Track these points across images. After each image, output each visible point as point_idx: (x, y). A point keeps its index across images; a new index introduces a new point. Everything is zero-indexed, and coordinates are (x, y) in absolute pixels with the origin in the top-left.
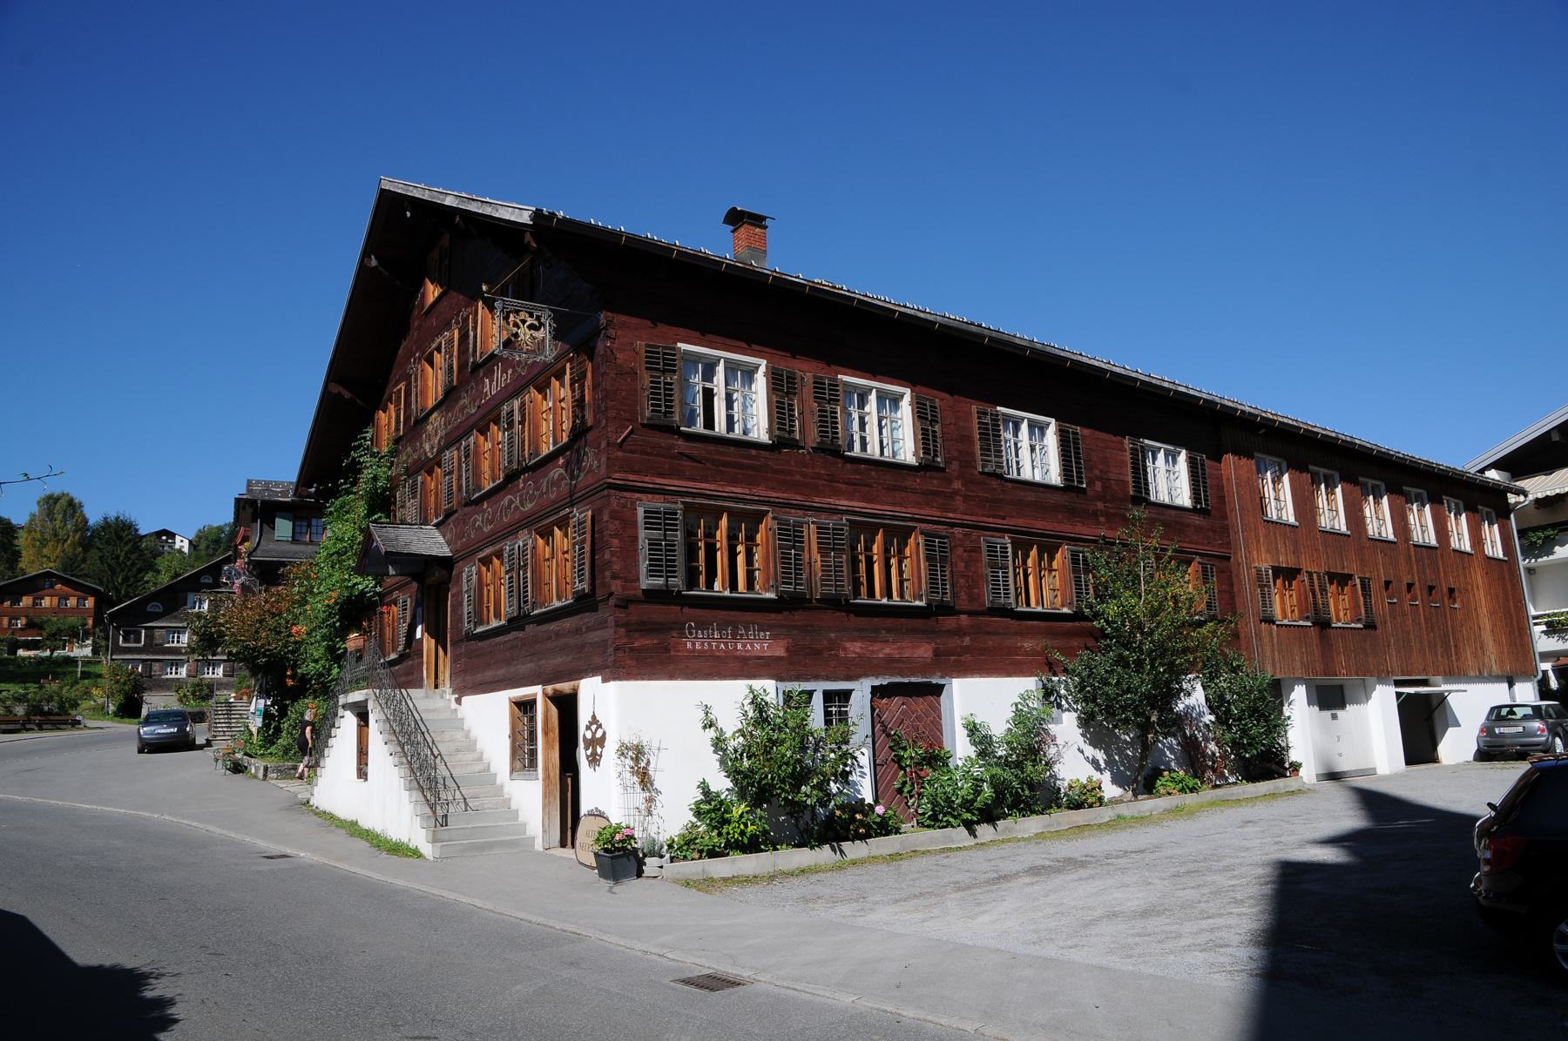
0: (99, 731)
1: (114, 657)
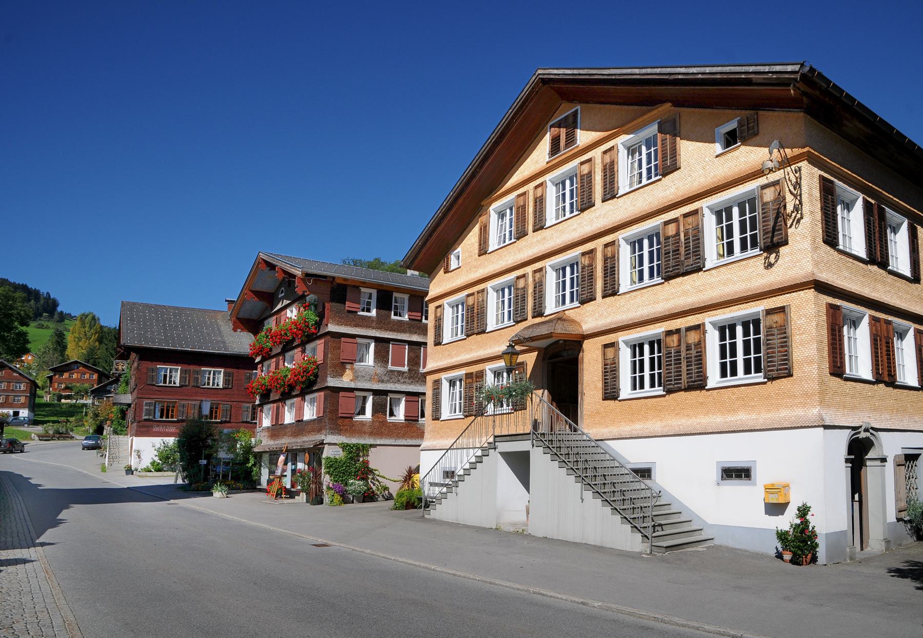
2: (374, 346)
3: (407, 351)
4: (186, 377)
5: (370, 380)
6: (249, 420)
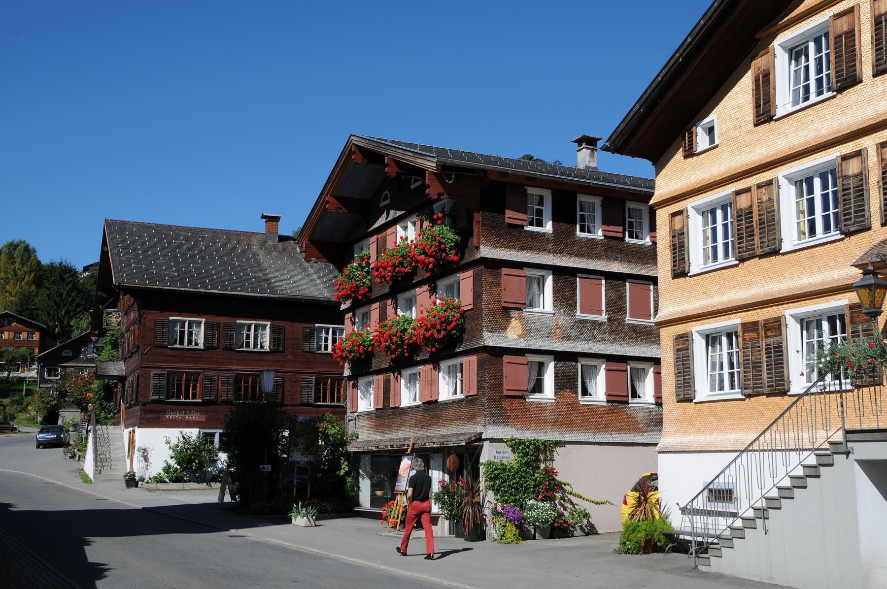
0: (27, 434)
1: (41, 386)
3: (603, 289)
4: (213, 335)
5: (549, 335)
6: (312, 401)
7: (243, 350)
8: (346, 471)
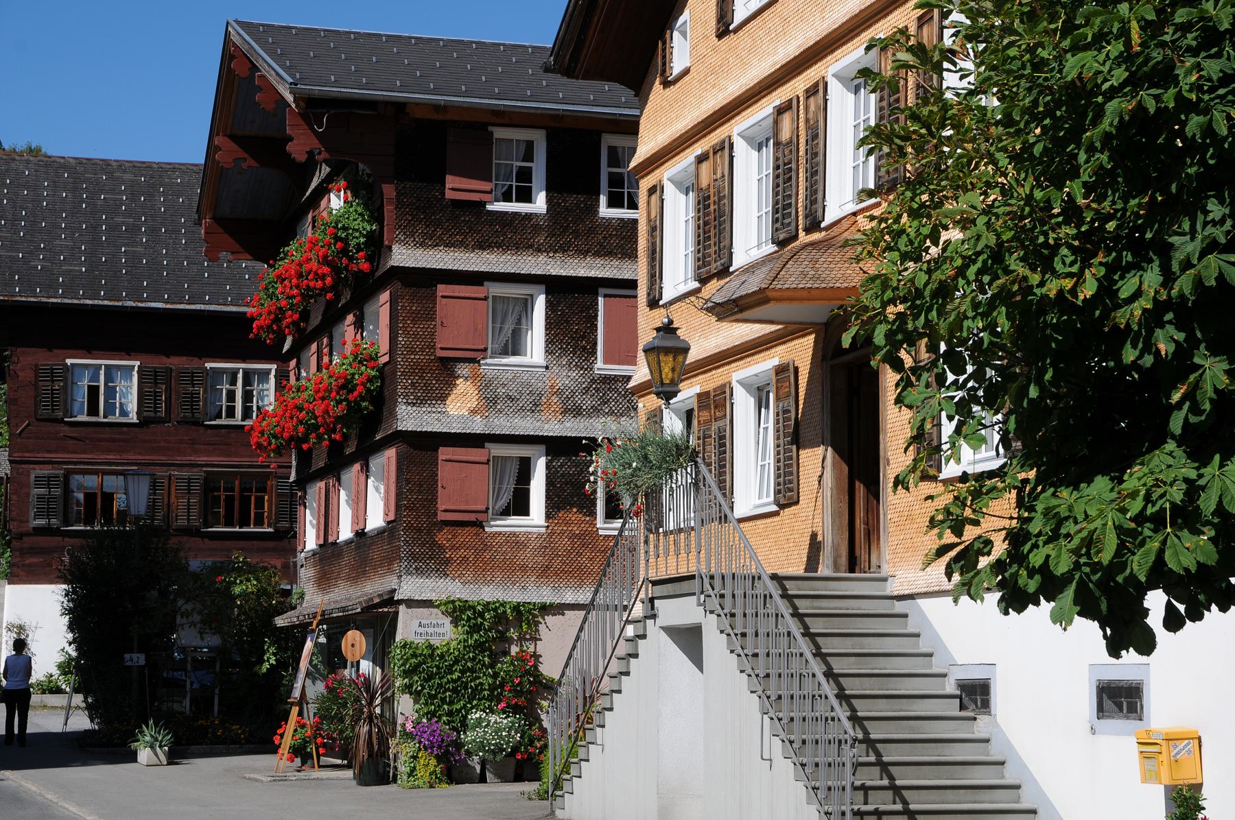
2: (544, 307)
7: (220, 423)
8: (271, 665)
